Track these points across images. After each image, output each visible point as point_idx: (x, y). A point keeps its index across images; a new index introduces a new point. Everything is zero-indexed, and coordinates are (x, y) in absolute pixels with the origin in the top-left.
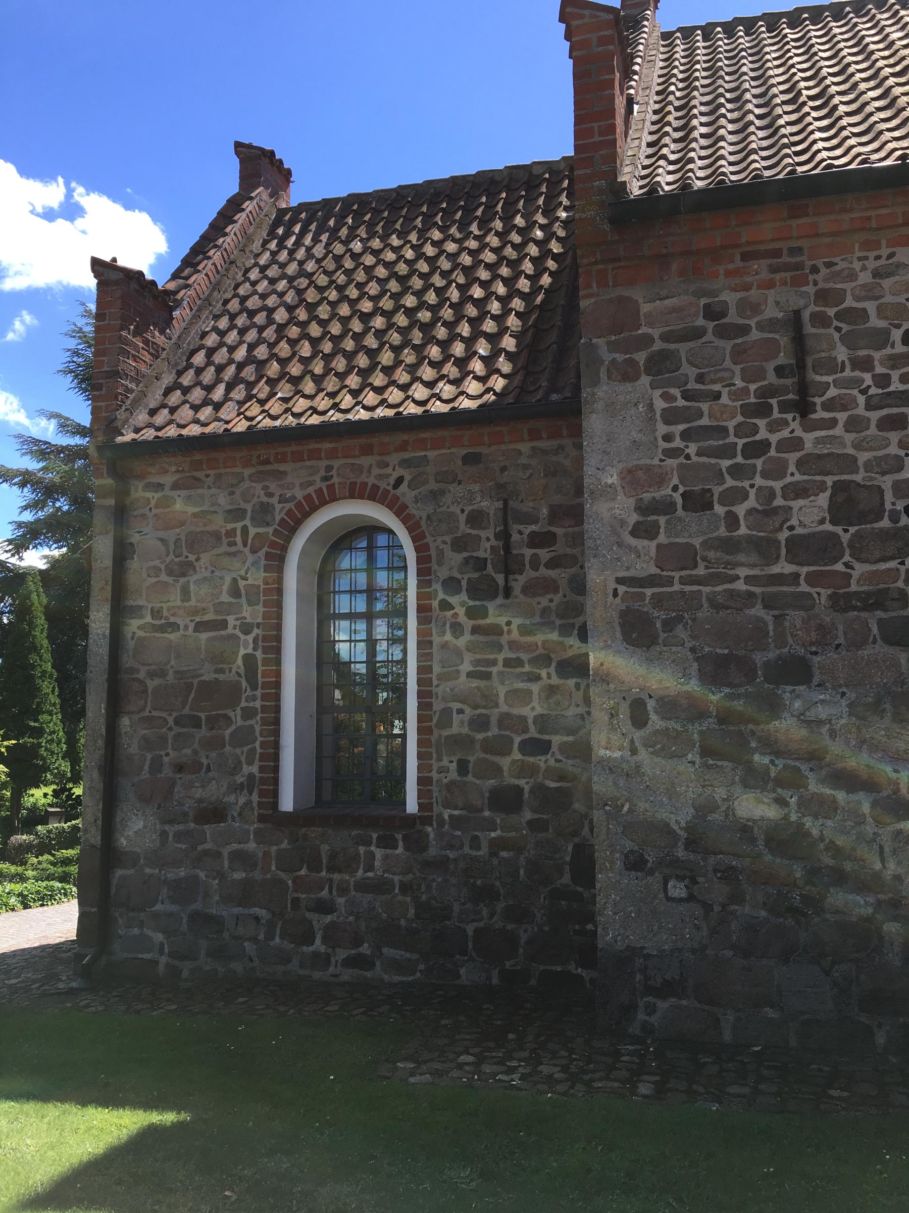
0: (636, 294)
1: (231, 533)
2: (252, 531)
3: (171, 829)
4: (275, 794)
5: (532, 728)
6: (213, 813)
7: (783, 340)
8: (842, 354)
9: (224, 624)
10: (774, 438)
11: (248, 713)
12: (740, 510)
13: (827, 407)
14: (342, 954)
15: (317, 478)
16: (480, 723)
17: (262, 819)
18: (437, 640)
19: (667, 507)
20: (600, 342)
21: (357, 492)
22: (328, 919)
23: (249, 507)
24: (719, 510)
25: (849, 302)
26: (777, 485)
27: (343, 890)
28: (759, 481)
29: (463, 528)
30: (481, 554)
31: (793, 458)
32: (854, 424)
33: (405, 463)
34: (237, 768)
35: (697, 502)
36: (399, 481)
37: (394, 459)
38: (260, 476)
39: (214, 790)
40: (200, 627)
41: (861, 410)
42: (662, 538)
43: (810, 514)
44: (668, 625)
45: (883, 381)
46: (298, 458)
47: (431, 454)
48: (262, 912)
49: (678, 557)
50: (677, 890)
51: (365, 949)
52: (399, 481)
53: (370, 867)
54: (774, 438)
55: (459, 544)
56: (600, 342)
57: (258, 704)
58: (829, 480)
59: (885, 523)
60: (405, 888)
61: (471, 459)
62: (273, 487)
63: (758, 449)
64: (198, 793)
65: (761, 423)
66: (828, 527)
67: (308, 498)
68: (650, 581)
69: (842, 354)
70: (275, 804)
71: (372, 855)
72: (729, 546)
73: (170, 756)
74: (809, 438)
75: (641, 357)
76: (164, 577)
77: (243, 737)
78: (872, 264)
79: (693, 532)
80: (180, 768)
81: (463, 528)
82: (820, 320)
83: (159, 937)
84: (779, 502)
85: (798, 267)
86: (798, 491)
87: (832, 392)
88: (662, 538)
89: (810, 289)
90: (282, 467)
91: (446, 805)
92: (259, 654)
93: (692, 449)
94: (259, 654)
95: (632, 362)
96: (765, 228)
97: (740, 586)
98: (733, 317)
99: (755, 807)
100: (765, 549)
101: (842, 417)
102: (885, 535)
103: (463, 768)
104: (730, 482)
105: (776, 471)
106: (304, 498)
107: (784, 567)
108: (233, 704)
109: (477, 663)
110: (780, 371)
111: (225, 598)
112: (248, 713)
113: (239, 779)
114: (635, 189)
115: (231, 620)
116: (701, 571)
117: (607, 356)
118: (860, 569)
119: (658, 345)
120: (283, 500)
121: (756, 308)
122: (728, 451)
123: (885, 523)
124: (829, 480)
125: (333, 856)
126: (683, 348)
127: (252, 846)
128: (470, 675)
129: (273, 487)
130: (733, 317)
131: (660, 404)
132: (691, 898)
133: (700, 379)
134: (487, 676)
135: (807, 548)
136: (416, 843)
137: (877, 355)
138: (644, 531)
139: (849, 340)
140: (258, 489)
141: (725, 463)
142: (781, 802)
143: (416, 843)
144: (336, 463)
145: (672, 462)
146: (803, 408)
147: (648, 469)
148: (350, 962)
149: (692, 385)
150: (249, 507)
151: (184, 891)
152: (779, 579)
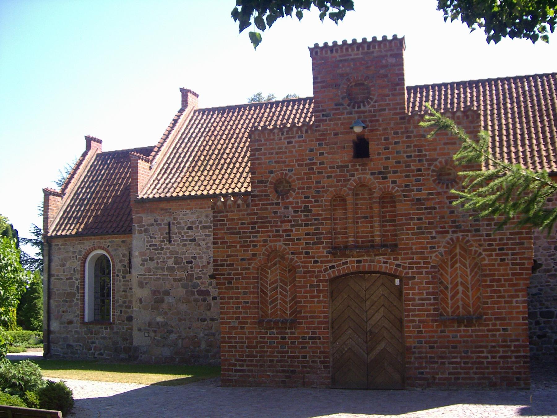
0: (143, 216)
1: (73, 257)
2: (78, 257)
3: (62, 326)
4: (84, 318)
5: (439, 300)
6: (71, 322)
7: (167, 227)
8: (176, 231)
9: (72, 279)
10: (165, 247)
11: (77, 299)
12: (159, 261)
13: (174, 241)
14: (97, 353)
15: (91, 245)
16: (124, 302)
17: (81, 323)
18: (116, 283)
19: (146, 260)
20: (136, 225)
21: (100, 248)
22: (94, 345)
23: (77, 251)
24: (155, 261)
25: (179, 220)
26: (165, 256)
27: (97, 339)
28: (162, 255)
29: (121, 258)
30: (125, 264)
31: (168, 251)
32: (178, 245)
33: (110, 242)
34: (75, 312)
35: (152, 259)
36: (109, 246)
37: (108, 241)
38: (79, 244)
39: (71, 317)
40: (67, 279)
41: (179, 242)
42: (146, 267)
43: (170, 263)
44: (146, 284)
45: (183, 237)
46: (87, 240)
47: (115, 240)
48: (82, 344)
49: (149, 270)
50: (146, 335)
51: (102, 351)
52: (109, 246)
53: (103, 334)
54: (165, 247)
55: (121, 261)
56: (136, 225)
57: (79, 297)
58: (174, 256)
59: (182, 265)
60: (110, 338)
61: (123, 242)
62: (82, 246)
63: (162, 249)
64: (67, 318)
65: (163, 244)
66: (173, 265)
67: (89, 249)
68: (144, 275)
69: (176, 231)
70: (84, 320)
71: (103, 331)
72: (157, 268)
73: (62, 309)
74: (171, 247)
75: (143, 229)
76: (59, 267)
77: (76, 305)
78: (183, 213)
79: (152, 265)
80: (63, 312)
81: (121, 258)
82: (173, 224)
83: (60, 349)
84: (165, 260)
85: (170, 212)
86: (169, 258)
87: (175, 238)
88: (146, 267)
89: (172, 217)
90: (84, 242)
91: (118, 320)
92: (79, 286)
93: (151, 248)
94: (79, 286)
95: (141, 230)
96: (163, 205)
97: (158, 276)
98: (159, 222)
99: (159, 319)
100: (163, 269)
101: (176, 243)
102: (182, 267)
103: (121, 311)
104: (157, 255)
105: (165, 254)
106: (283, 16)
107: (166, 273)
108: (74, 297)
109: (124, 289)
110: (166, 233)
111: (72, 272)
112: (77, 299)
113: (76, 314)
114: (140, 197)
115: (74, 278)
116: (152, 273)
117: (137, 228)
118: (178, 273)
119: (146, 227)
120: (84, 250)
121: (163, 220)
122: (157, 249)
123: (182, 265)
124: (174, 256)
125: (95, 332)
126: (150, 227)
127: (78, 329)
128: (123, 291)
129: (82, 246)
130: (159, 222)
131: (146, 239)
132: (148, 336)
133: (153, 234)
134: (126, 291)
135: (171, 269)
136: (112, 329)
137: (182, 232)
138: (143, 265)
139: (178, 228)
140: (79, 247)
141: (157, 252)
142: (164, 318)
143: (112, 329)
144: (96, 241)
145: (148, 251)
146: (170, 241)
147: (144, 252)
148: (99, 354)
149: (152, 235)
150: (77, 251)
151: (65, 339)
152: (164, 275)
